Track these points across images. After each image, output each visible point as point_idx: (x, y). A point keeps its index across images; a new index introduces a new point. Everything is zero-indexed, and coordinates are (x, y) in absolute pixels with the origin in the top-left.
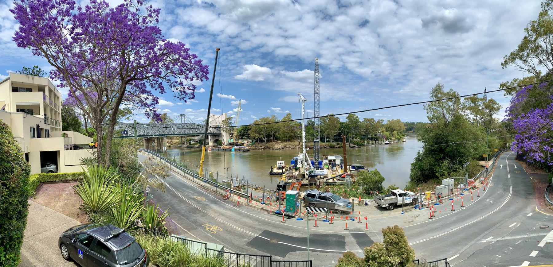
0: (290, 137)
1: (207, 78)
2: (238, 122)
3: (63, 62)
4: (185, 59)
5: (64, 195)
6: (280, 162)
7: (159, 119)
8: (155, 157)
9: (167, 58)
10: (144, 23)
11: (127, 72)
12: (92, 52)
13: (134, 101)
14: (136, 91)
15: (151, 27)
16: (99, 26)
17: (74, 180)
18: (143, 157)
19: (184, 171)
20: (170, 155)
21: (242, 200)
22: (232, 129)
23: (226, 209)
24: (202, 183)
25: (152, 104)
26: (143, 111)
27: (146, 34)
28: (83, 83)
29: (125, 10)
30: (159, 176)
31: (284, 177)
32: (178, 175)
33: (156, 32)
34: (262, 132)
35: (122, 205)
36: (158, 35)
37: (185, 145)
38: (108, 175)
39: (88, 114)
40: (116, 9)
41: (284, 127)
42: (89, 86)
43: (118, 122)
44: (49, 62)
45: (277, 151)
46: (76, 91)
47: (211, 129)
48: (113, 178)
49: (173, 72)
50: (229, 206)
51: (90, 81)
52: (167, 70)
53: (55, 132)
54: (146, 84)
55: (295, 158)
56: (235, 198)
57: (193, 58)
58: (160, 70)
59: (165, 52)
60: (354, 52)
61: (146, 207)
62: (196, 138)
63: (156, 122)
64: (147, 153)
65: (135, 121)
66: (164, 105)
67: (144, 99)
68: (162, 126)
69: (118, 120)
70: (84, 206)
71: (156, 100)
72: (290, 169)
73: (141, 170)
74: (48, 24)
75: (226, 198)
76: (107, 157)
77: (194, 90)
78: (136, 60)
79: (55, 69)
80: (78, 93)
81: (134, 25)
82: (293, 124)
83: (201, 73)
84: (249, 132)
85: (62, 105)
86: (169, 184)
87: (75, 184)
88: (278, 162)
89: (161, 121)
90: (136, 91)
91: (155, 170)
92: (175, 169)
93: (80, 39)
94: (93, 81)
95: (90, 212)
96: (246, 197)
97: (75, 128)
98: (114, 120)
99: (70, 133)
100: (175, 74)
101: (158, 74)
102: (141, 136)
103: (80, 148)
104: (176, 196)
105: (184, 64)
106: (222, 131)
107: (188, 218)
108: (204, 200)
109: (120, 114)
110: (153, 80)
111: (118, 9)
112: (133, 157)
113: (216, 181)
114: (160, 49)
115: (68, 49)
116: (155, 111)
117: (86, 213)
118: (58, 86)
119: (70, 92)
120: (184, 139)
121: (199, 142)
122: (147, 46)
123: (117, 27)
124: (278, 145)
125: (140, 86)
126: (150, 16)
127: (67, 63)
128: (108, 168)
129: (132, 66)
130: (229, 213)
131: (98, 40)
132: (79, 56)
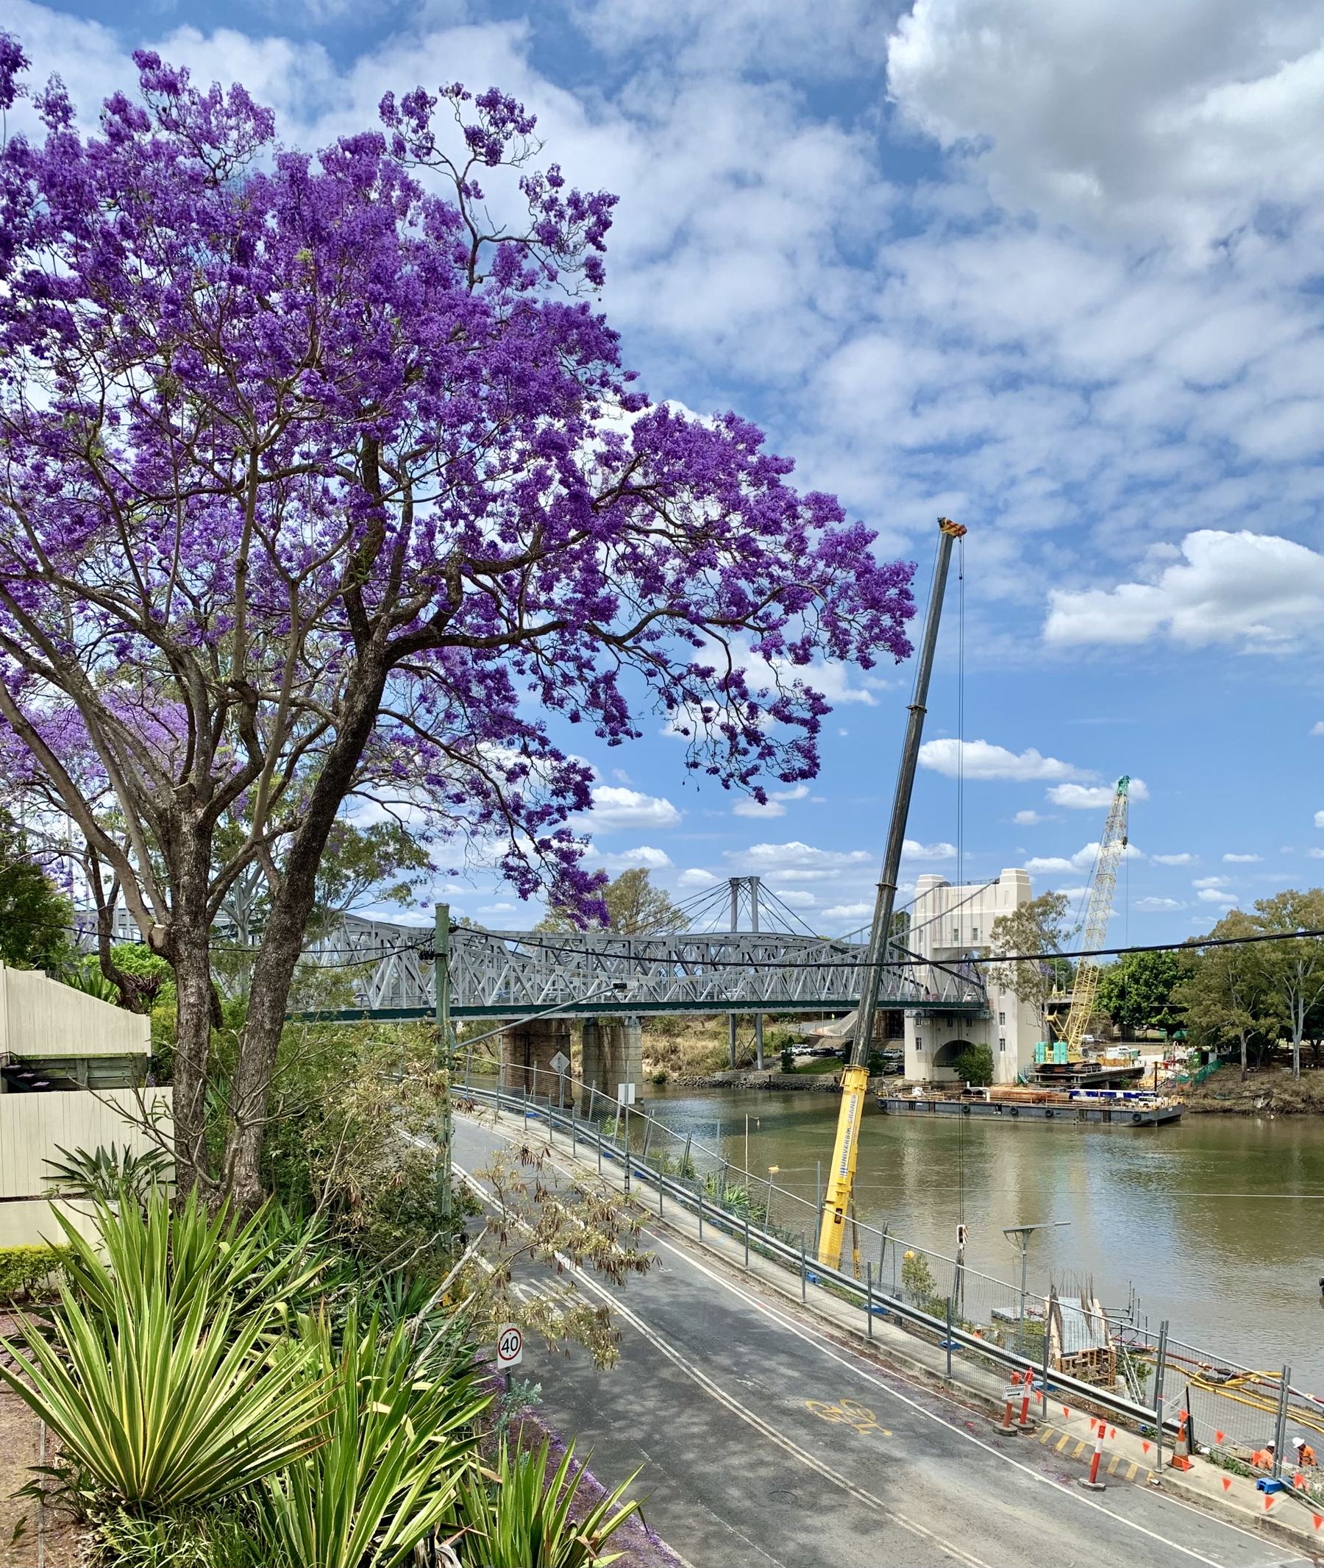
1: (901, 648)
4: (766, 530)
8: (565, 1143)
9: (649, 518)
10: (505, 281)
11: (395, 588)
12: (151, 429)
13: (437, 781)
14: (450, 717)
18: (491, 1141)
19: (743, 1241)
20: (659, 1138)
21: (1122, 1444)
22: (1060, 971)
23: (1014, 1493)
24: (857, 1320)
27: (518, 353)
28: (84, 633)
30: (579, 1261)
33: (583, 342)
34: (1273, 998)
35: (337, 1453)
36: (596, 367)
37: (759, 1075)
38: (241, 1264)
43: (335, 919)
47: (922, 973)
49: (684, 612)
50: (1030, 1475)
52: (646, 590)
54: (513, 678)
56: (1081, 1427)
57: (819, 522)
58: (602, 592)
59: (637, 479)
60: (177, 1326)
61: (492, 1461)
64: (519, 1121)
65: (443, 909)
66: (627, 822)
67: (500, 777)
68: (617, 949)
70: (62, 1474)
71: (576, 788)
75: (1014, 1428)
77: (813, 726)
83: (864, 618)
84: (1178, 994)
86: (653, 1316)
89: (605, 919)
90: (450, 717)
92: (689, 1223)
93: (64, 323)
95: (108, 1507)
96: (1150, 1430)
97: (22, 941)
98: (299, 910)
104: (691, 1396)
106: (992, 990)
107: (763, 1534)
108: (868, 1430)
110: (562, 656)
112: (421, 1143)
113: (948, 1309)
114: (605, 460)
116: (567, 856)
117: (81, 1521)
120: (748, 1037)
121: (849, 1050)
122: (528, 431)
123: (327, 288)
125: (477, 691)
128: (246, 1218)
129: (426, 553)
130: (1027, 1519)
131: (192, 352)
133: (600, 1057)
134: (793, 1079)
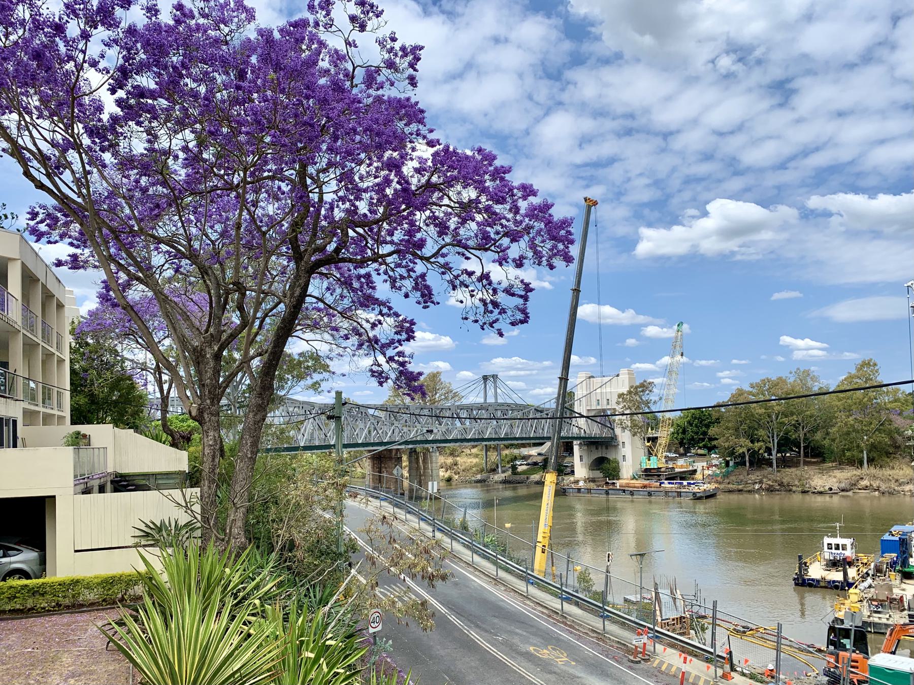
0: (873, 447)
1: (568, 259)
2: (674, 397)
3: (82, 182)
4: (498, 202)
5: (66, 659)
6: (834, 541)
7: (415, 390)
8: (401, 514)
9: (441, 198)
10: (369, 86)
11: (314, 235)
12: (193, 160)
13: (336, 329)
14: (342, 297)
15: (390, 101)
16: (220, 78)
17: (108, 603)
18: (363, 513)
19: (495, 563)
20: (450, 509)
22: (653, 421)
25: (392, 342)
26: (367, 362)
28: (157, 260)
29: (311, 41)
30: (413, 577)
31: (854, 598)
32: (476, 573)
33: (407, 114)
34: (761, 432)
36: (414, 127)
37: (499, 476)
38: (236, 579)
39: (172, 369)
40: (281, 31)
41: (848, 410)
42: (177, 271)
43: (282, 399)
44: (27, 174)
45: (819, 499)
46: (127, 285)
47: (582, 422)
48: (257, 587)
49: (459, 244)
51: (184, 256)
52: (441, 234)
53: (40, 429)
54: (375, 277)
55: (895, 529)
58: (419, 236)
59: (434, 179)
62: (534, 451)
63: (407, 400)
64: (376, 503)
65: (339, 394)
67: (367, 326)
68: (426, 412)
69: (282, 393)
71: (407, 330)
72: (878, 570)
73: (353, 557)
74: (27, 42)
76: (236, 518)
77: (525, 298)
78: (342, 199)
79: (50, 202)
80: (137, 293)
81: (337, 87)
82: (885, 399)
84: (713, 431)
85: (72, 332)
87: (110, 616)
88: (827, 540)
89: (424, 394)
90: (342, 297)
91: (401, 556)
92: (467, 554)
93: (151, 110)
94: (193, 256)
96: (710, 658)
97: (122, 414)
98: (266, 393)
99: (102, 433)
100: (466, 247)
101: (412, 247)
102: (357, 445)
103: (138, 488)
104: (470, 646)
105: (493, 218)
106: (618, 431)
109: (289, 371)
110: (399, 265)
111: (289, 33)
113: (602, 596)
114: (418, 171)
115: (104, 138)
118: (59, 264)
119: (108, 288)
120: (493, 456)
122: (380, 158)
123: (282, 91)
124: (825, 479)
125: (356, 285)
126: (391, 65)
127: (98, 185)
128: (238, 555)
129: (329, 217)
132: (145, 169)
133: (418, 468)
134: (517, 478)
